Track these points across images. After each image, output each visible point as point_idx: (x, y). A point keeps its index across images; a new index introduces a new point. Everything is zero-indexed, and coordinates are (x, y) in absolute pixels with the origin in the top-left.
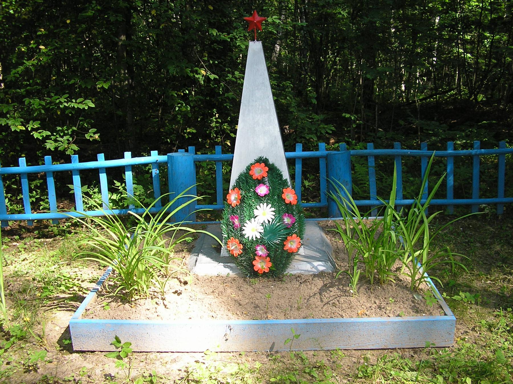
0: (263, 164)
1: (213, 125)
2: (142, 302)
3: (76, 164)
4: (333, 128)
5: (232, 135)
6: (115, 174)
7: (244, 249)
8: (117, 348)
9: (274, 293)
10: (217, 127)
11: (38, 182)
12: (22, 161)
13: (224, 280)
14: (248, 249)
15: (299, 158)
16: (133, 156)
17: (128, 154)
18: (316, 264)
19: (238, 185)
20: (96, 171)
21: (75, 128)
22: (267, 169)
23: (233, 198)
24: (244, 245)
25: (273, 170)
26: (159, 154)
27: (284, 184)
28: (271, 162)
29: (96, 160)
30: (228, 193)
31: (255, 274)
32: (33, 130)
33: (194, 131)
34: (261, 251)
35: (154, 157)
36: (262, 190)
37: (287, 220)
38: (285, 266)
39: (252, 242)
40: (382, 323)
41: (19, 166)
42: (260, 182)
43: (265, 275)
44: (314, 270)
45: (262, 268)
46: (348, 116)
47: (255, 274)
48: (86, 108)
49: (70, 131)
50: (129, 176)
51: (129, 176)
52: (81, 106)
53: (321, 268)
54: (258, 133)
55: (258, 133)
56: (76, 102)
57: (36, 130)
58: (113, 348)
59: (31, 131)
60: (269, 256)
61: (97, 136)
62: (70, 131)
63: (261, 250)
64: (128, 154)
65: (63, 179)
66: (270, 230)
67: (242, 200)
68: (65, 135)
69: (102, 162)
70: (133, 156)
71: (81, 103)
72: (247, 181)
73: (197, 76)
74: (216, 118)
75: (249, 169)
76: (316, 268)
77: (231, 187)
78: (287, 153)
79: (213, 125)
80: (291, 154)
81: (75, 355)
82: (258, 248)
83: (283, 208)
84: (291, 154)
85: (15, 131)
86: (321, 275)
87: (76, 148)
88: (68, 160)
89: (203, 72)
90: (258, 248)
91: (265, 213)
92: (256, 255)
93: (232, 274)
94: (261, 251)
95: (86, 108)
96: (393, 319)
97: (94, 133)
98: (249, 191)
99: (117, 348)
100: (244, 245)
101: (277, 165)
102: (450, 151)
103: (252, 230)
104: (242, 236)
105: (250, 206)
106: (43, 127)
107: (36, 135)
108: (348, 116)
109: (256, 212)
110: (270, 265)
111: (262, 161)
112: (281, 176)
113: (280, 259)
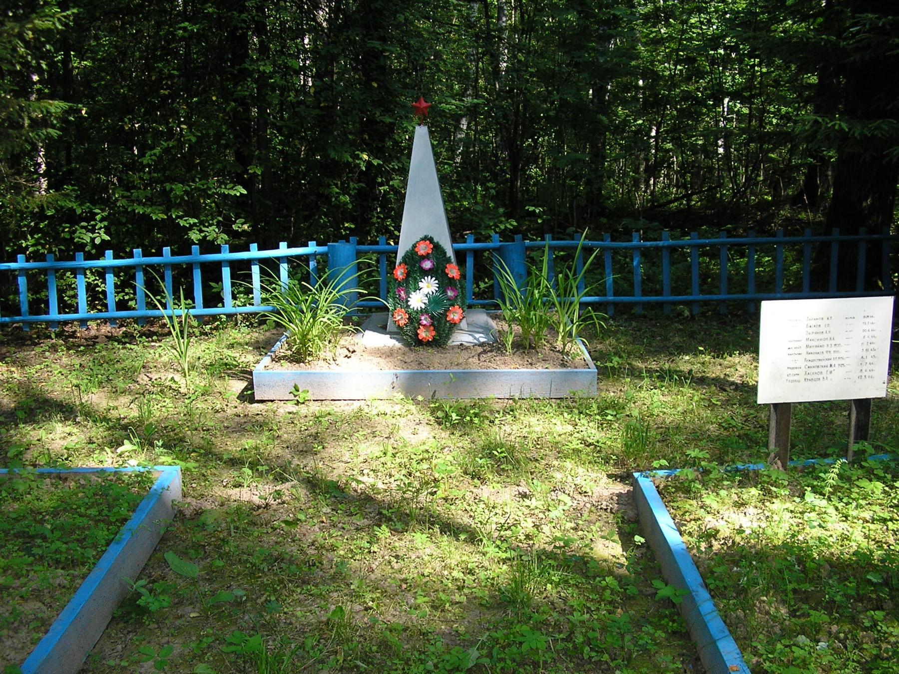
0: (428, 242)
1: (374, 220)
2: (315, 362)
3: (226, 255)
4: (515, 224)
5: (396, 233)
6: (270, 267)
7: (409, 319)
8: (295, 396)
9: (436, 361)
10: (378, 223)
11: (183, 275)
12: (167, 250)
13: (389, 354)
14: (414, 319)
15: (470, 250)
16: (289, 247)
17: (283, 245)
18: (477, 336)
19: (405, 260)
20: (248, 263)
21: (220, 219)
22: (432, 246)
23: (400, 273)
24: (410, 314)
25: (437, 247)
26: (318, 245)
27: (448, 260)
28: (435, 240)
29: (249, 250)
30: (394, 268)
31: (419, 343)
32: (178, 217)
33: (353, 226)
34: (425, 320)
35: (312, 248)
36: (427, 265)
37: (450, 293)
38: (448, 337)
39: (417, 312)
40: (532, 374)
41: (162, 256)
42: (425, 257)
43: (429, 344)
44: (475, 341)
45: (425, 338)
46: (532, 209)
47: (419, 343)
48: (238, 194)
49: (215, 221)
50: (284, 268)
51: (284, 268)
52: (232, 193)
53: (482, 340)
54: (423, 217)
55: (423, 217)
56: (226, 188)
57: (181, 217)
58: (291, 397)
59: (176, 219)
60: (432, 325)
61: (246, 227)
62: (215, 221)
63: (425, 319)
64: (283, 245)
65: (212, 272)
66: (433, 301)
67: (408, 275)
68: (211, 225)
69: (254, 252)
70: (289, 247)
71: (232, 188)
72: (412, 258)
73: (357, 162)
74: (377, 213)
75: (414, 246)
76: (478, 340)
77: (397, 264)
78: (456, 245)
79: (374, 220)
80: (461, 246)
81: (256, 405)
82: (423, 318)
83: (445, 282)
84: (461, 246)
85: (156, 219)
86: (482, 345)
87: (225, 237)
88: (218, 250)
89: (365, 157)
90: (423, 318)
91: (429, 286)
92: (420, 324)
93: (398, 345)
94: (425, 320)
95: (238, 194)
96: (540, 370)
97: (242, 224)
98: (415, 266)
99: (295, 396)
100: (410, 314)
101: (442, 243)
102: (635, 243)
103: (417, 301)
104: (408, 306)
105: (415, 279)
106: (188, 214)
107: (182, 223)
108: (532, 209)
109: (421, 285)
110: (434, 333)
111: (428, 239)
112: (445, 253)
113: (443, 329)
